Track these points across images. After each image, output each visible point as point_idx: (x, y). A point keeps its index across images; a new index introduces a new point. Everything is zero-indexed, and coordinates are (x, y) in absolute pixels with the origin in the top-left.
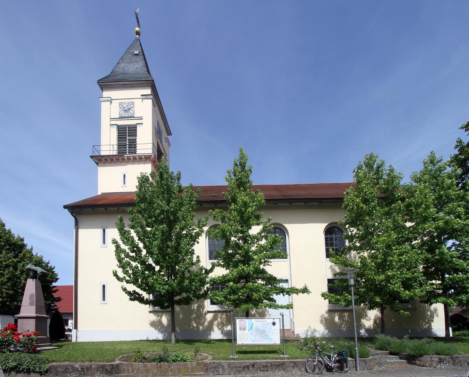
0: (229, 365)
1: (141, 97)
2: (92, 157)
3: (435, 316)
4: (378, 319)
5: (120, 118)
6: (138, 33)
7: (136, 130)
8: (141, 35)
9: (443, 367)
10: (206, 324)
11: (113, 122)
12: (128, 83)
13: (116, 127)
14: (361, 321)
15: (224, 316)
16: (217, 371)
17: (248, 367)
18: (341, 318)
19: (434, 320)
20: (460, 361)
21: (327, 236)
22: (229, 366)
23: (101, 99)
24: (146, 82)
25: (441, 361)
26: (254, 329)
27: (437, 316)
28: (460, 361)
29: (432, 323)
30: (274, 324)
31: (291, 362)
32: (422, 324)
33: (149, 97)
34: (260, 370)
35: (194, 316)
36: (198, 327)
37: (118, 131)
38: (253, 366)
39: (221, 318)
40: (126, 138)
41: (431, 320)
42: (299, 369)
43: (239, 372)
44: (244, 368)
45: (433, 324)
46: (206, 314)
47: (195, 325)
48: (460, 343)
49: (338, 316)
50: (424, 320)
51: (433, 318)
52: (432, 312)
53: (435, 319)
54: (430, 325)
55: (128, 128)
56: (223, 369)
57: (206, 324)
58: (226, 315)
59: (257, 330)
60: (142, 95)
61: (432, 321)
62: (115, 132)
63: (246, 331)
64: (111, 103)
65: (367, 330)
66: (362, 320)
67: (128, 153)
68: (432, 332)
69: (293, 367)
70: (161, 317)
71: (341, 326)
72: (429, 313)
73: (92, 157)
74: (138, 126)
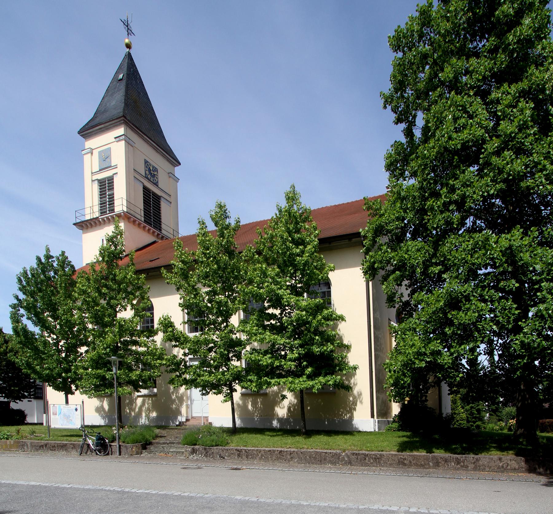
0: (31, 443)
1: (114, 140)
2: (74, 224)
3: (358, 403)
4: (293, 405)
5: (100, 170)
6: (128, 46)
7: (113, 182)
8: (133, 46)
9: (195, 458)
10: (137, 410)
11: (95, 177)
12: (102, 126)
13: (96, 182)
14: (274, 410)
15: (150, 402)
16: (24, 448)
17: (42, 446)
18: (254, 404)
19: (357, 408)
20: (213, 453)
21: (329, 290)
22: (31, 445)
23: (83, 152)
24: (118, 120)
25: (194, 452)
26: (62, 414)
27: (361, 402)
28: (213, 453)
29: (354, 412)
30: (76, 410)
31: (71, 444)
32: (342, 413)
33: (121, 138)
34: (51, 450)
35: (127, 401)
36: (130, 413)
37: (100, 186)
38: (46, 446)
39: (148, 404)
40: (106, 193)
41: (351, 409)
42: (77, 451)
43: (37, 450)
44: (40, 447)
45: (355, 414)
46: (136, 399)
47: (128, 411)
48: (341, 436)
49: (252, 402)
50: (345, 408)
51: (356, 405)
52: (354, 398)
53: (359, 406)
54: (352, 414)
55: (108, 181)
56: (27, 447)
57: (137, 410)
58: (152, 400)
59: (65, 415)
60: (115, 138)
61: (355, 409)
62: (96, 186)
63: (57, 416)
64: (92, 154)
65: (280, 420)
66: (276, 408)
67: (108, 212)
68: (353, 425)
69: (72, 448)
70: (103, 402)
71: (254, 414)
72: (351, 399)
73: (74, 224)
74: (115, 176)
